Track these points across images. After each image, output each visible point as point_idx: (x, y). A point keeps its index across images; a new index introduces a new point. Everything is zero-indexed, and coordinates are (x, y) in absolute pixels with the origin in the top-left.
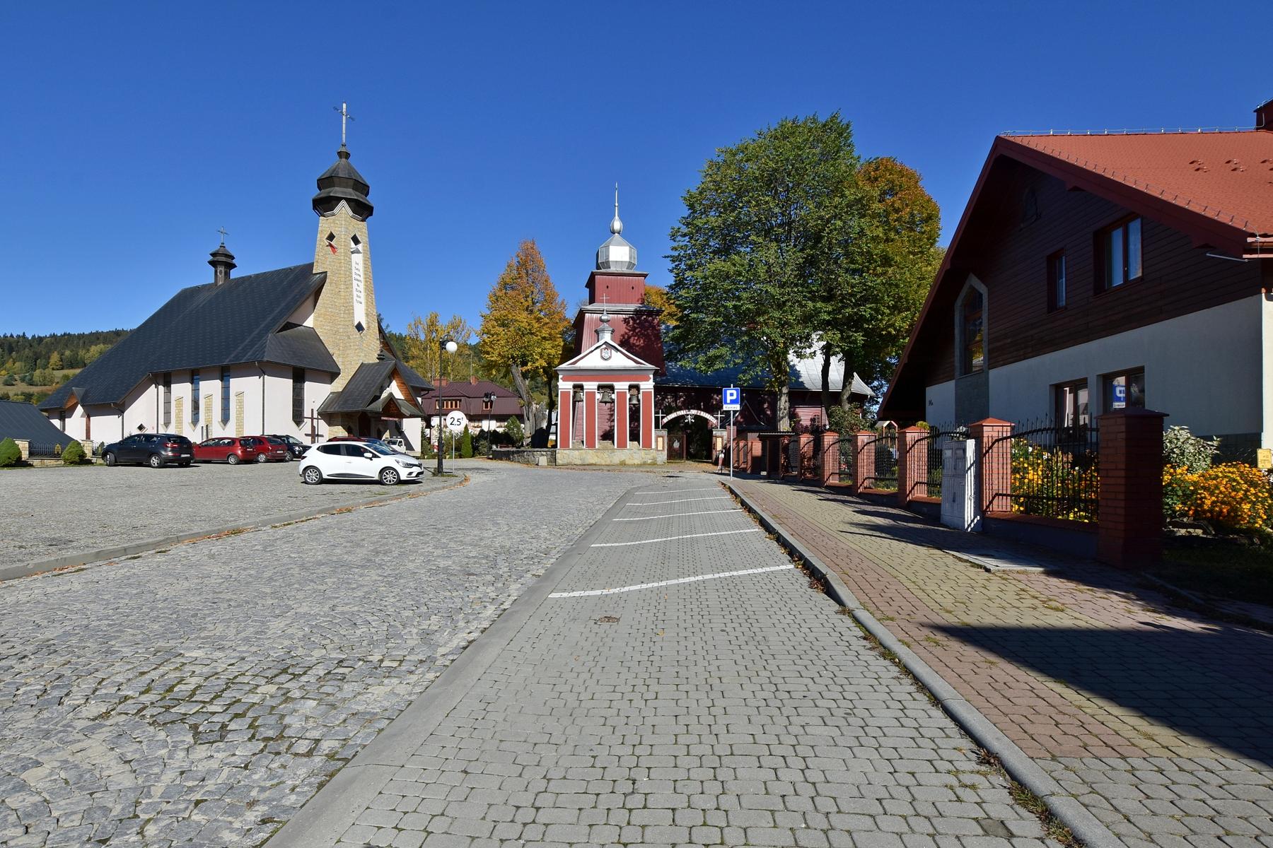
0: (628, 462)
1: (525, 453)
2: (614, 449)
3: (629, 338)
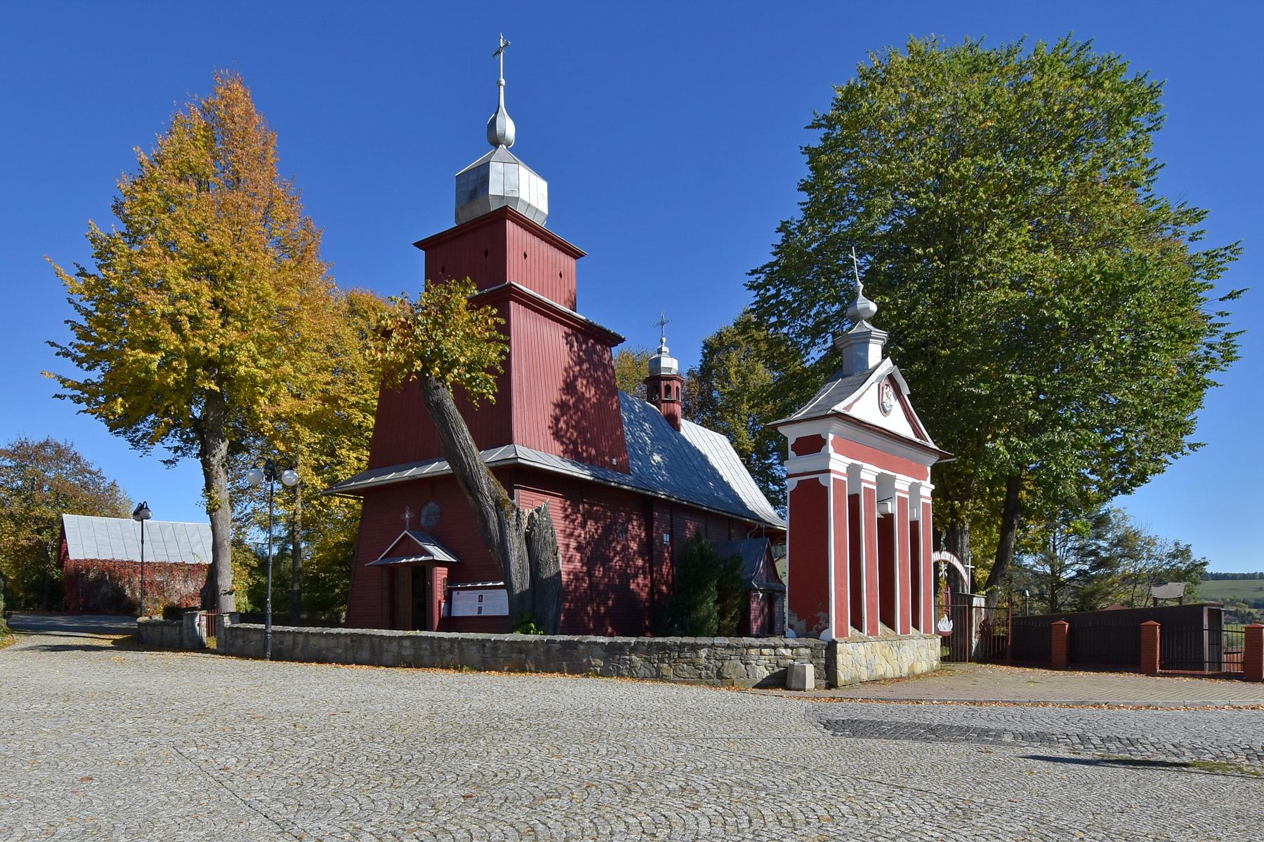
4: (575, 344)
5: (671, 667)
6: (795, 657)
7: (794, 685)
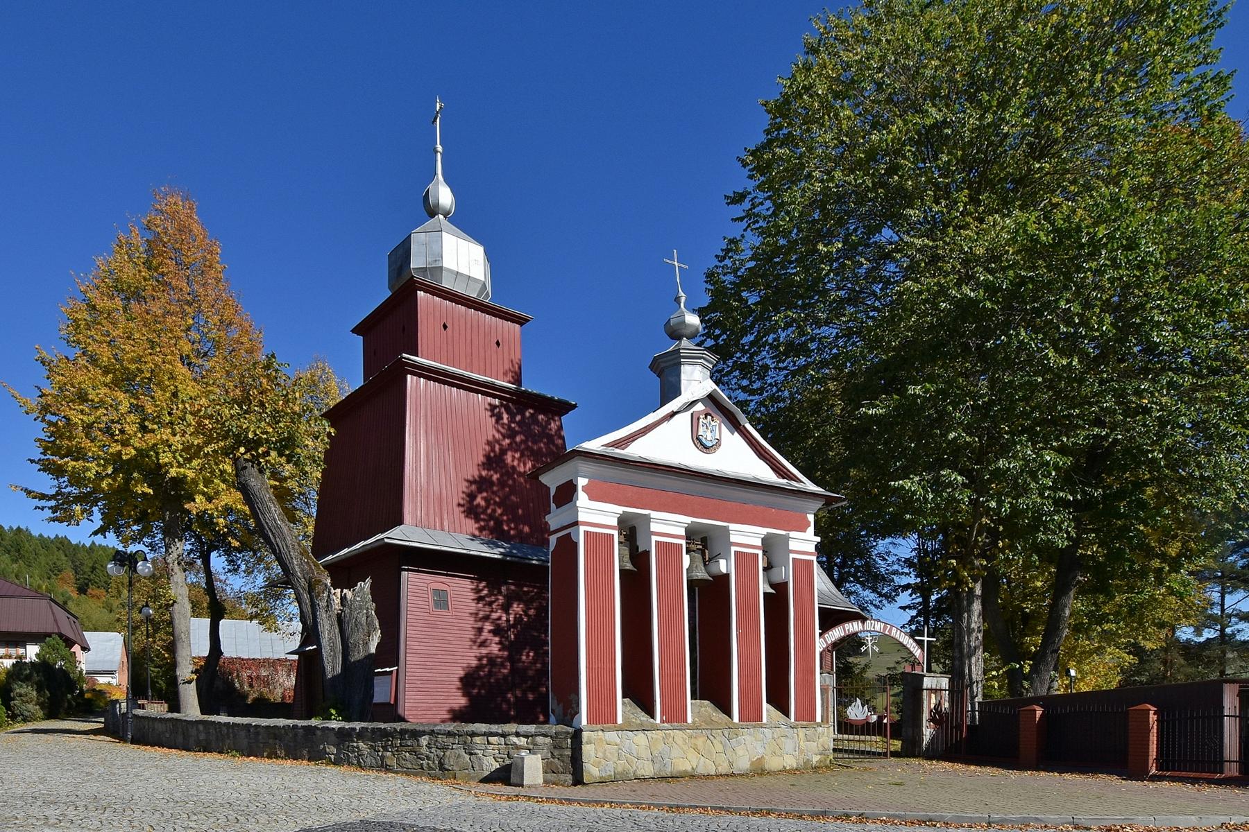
0: (773, 764)
1: (424, 741)
2: (736, 727)
3: (503, 452)
4: (505, 416)
5: (394, 755)
6: (531, 747)
7: (513, 779)
